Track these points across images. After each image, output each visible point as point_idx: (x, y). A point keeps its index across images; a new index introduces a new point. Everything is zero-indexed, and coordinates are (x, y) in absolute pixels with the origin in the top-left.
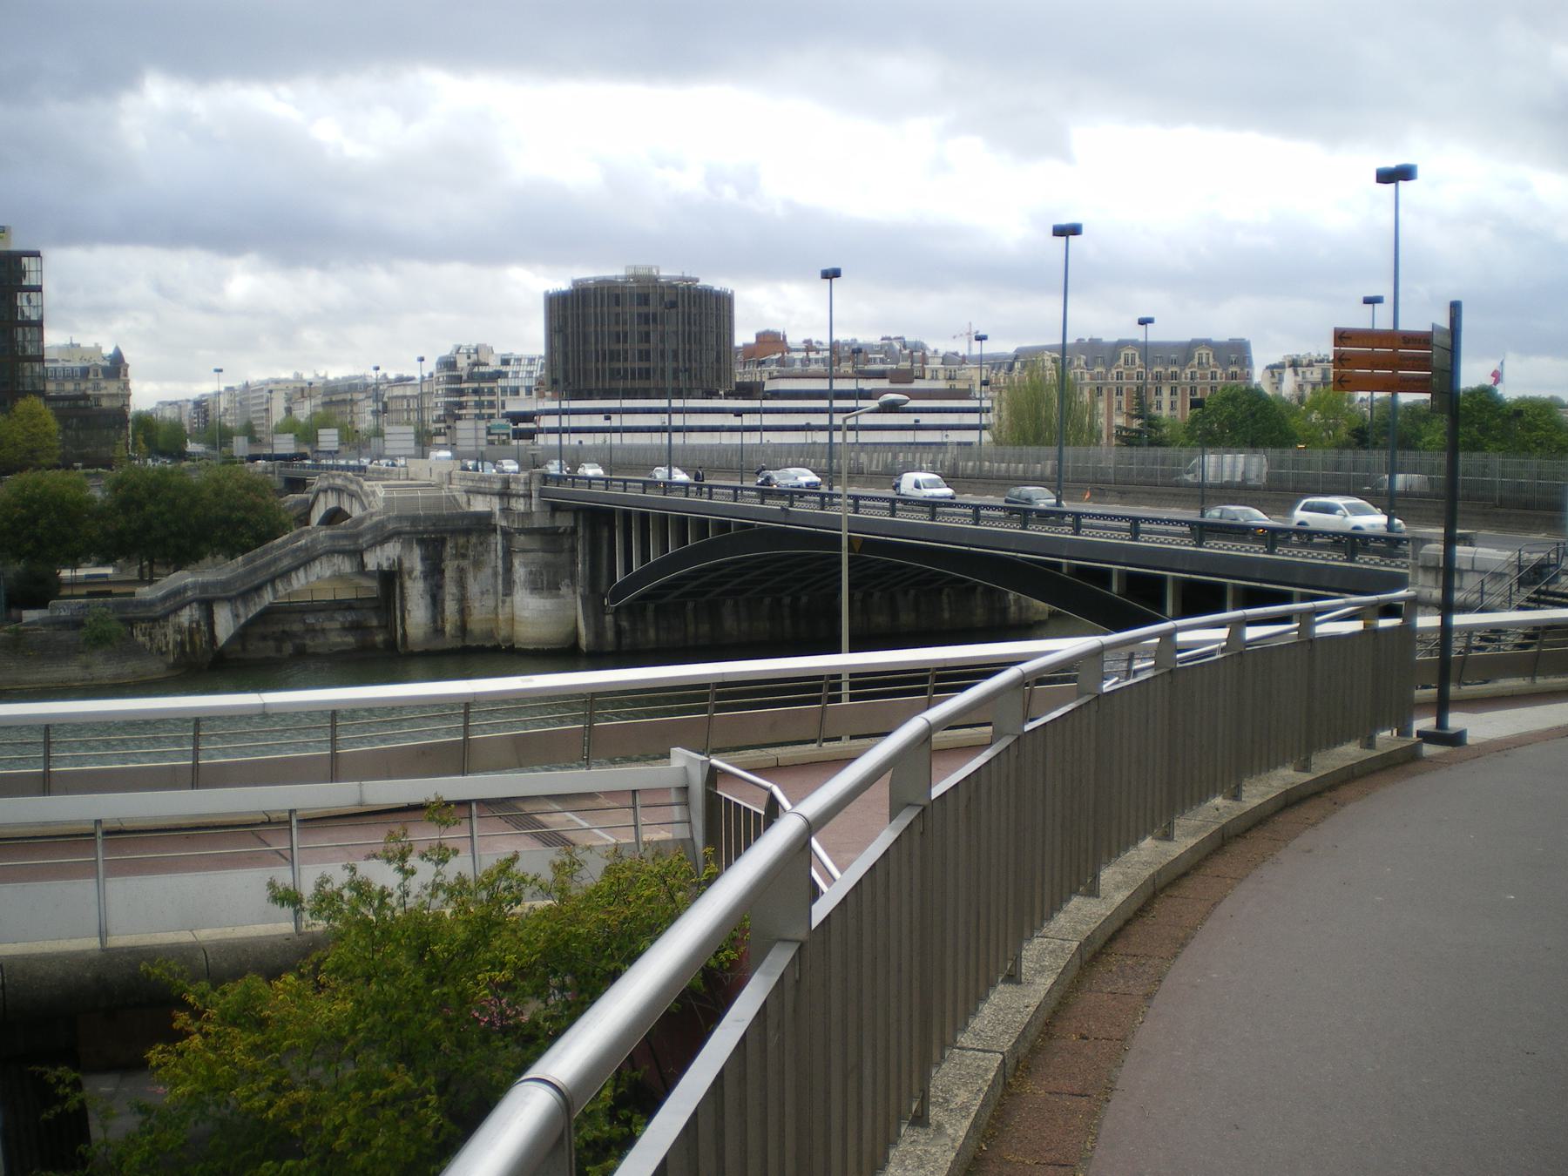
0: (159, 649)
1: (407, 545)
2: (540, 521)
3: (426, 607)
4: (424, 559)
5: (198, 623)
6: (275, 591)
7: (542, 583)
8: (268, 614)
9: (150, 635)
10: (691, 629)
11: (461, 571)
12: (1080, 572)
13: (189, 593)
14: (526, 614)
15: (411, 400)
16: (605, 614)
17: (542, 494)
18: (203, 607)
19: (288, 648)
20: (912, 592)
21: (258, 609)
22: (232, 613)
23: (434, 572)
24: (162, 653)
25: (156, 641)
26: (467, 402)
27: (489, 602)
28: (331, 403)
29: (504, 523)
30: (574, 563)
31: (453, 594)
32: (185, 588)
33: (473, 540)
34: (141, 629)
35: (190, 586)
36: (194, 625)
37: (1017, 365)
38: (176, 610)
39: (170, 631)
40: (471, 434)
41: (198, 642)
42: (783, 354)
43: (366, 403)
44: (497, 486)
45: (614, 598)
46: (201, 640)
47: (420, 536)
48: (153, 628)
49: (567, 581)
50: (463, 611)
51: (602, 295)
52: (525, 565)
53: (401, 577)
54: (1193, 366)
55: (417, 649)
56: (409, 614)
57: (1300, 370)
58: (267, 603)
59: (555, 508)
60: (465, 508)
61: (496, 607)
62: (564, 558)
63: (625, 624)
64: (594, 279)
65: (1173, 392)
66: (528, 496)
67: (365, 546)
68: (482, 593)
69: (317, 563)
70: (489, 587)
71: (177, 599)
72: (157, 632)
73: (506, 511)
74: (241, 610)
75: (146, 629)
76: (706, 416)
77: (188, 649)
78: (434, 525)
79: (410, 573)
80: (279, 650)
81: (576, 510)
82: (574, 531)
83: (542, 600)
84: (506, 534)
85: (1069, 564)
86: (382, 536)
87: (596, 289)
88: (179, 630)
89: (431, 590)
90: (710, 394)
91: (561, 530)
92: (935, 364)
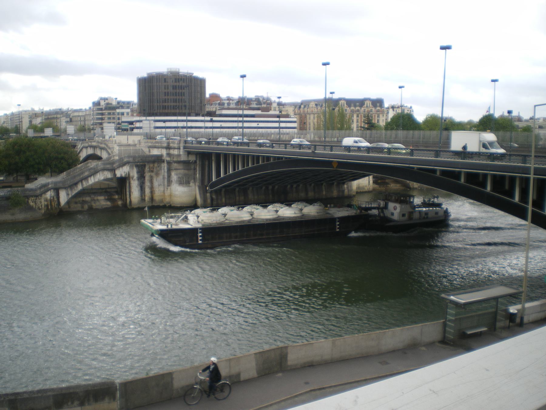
0: (39, 208)
1: (131, 167)
2: (184, 158)
3: (139, 191)
4: (138, 172)
5: (53, 198)
6: (82, 185)
7: (183, 181)
8: (84, 192)
9: (35, 202)
10: (237, 198)
11: (151, 177)
12: (444, 173)
13: (50, 186)
14: (177, 193)
15: (82, 117)
16: (207, 193)
17: (185, 148)
18: (55, 191)
19: (86, 207)
20: (313, 185)
21: (76, 192)
22: (66, 193)
23: (142, 177)
24: (40, 209)
25: (37, 204)
26: (104, 117)
27: (162, 189)
28: (48, 118)
29: (168, 159)
30: (195, 174)
31: (148, 186)
32: (48, 184)
33: (156, 165)
34: (32, 200)
35: (50, 183)
36: (52, 198)
37: (302, 106)
38: (45, 192)
39: (43, 200)
40: (148, 126)
41: (53, 204)
42: (220, 101)
43: (63, 118)
44: (165, 145)
45: (211, 187)
46: (54, 204)
47: (136, 164)
48: (36, 199)
49: (193, 181)
50: (152, 192)
51: (159, 79)
52: (177, 175)
53: (129, 179)
54: (364, 107)
55: (135, 207)
56: (132, 193)
57: (395, 109)
58: (79, 190)
59: (189, 153)
60: (147, 153)
61: (164, 191)
62: (191, 172)
63: (214, 197)
64: (156, 73)
65: (358, 116)
66: (179, 148)
67: (116, 167)
68: (159, 185)
69: (98, 174)
70: (161, 183)
71: (45, 188)
72: (38, 201)
73: (169, 155)
74: (70, 192)
75: (33, 200)
76: (197, 123)
77: (49, 207)
78: (141, 159)
79: (133, 178)
80: (83, 207)
81: (197, 154)
82: (195, 162)
83: (183, 188)
84: (169, 163)
85: (440, 170)
86: (123, 164)
87: (157, 76)
88: (46, 200)
89: (140, 184)
90: (197, 115)
91: (191, 161)
92: (275, 105)
